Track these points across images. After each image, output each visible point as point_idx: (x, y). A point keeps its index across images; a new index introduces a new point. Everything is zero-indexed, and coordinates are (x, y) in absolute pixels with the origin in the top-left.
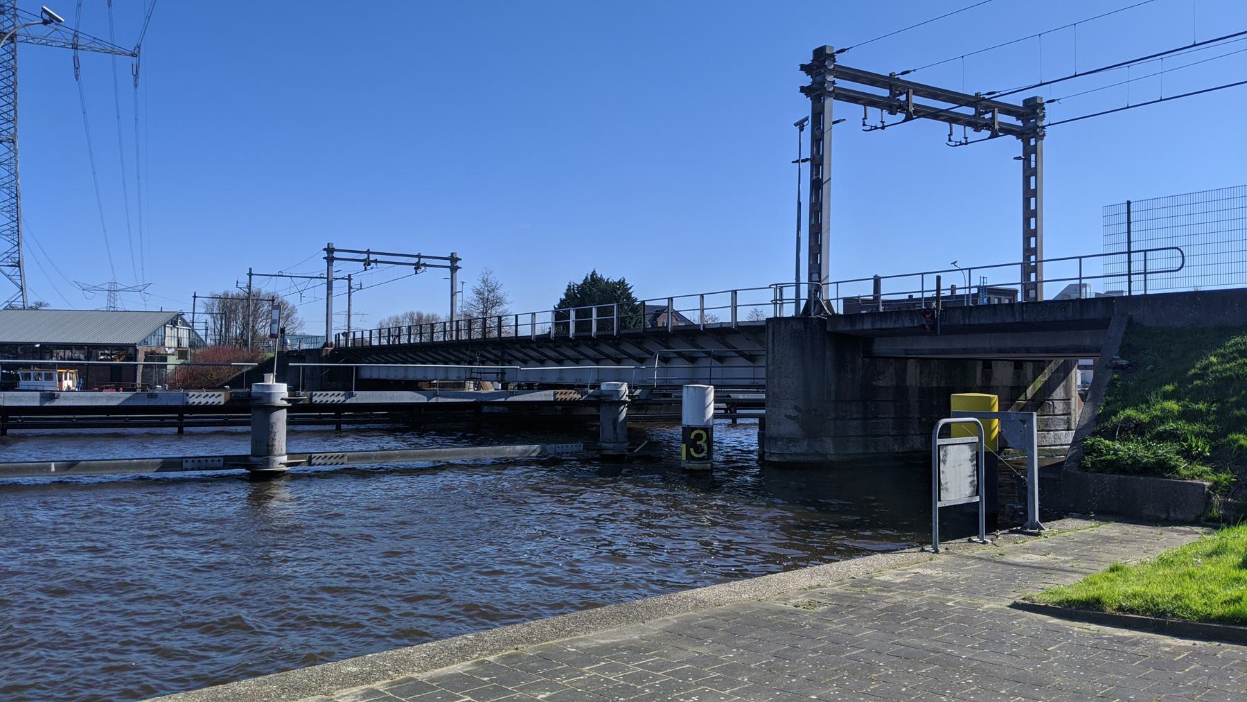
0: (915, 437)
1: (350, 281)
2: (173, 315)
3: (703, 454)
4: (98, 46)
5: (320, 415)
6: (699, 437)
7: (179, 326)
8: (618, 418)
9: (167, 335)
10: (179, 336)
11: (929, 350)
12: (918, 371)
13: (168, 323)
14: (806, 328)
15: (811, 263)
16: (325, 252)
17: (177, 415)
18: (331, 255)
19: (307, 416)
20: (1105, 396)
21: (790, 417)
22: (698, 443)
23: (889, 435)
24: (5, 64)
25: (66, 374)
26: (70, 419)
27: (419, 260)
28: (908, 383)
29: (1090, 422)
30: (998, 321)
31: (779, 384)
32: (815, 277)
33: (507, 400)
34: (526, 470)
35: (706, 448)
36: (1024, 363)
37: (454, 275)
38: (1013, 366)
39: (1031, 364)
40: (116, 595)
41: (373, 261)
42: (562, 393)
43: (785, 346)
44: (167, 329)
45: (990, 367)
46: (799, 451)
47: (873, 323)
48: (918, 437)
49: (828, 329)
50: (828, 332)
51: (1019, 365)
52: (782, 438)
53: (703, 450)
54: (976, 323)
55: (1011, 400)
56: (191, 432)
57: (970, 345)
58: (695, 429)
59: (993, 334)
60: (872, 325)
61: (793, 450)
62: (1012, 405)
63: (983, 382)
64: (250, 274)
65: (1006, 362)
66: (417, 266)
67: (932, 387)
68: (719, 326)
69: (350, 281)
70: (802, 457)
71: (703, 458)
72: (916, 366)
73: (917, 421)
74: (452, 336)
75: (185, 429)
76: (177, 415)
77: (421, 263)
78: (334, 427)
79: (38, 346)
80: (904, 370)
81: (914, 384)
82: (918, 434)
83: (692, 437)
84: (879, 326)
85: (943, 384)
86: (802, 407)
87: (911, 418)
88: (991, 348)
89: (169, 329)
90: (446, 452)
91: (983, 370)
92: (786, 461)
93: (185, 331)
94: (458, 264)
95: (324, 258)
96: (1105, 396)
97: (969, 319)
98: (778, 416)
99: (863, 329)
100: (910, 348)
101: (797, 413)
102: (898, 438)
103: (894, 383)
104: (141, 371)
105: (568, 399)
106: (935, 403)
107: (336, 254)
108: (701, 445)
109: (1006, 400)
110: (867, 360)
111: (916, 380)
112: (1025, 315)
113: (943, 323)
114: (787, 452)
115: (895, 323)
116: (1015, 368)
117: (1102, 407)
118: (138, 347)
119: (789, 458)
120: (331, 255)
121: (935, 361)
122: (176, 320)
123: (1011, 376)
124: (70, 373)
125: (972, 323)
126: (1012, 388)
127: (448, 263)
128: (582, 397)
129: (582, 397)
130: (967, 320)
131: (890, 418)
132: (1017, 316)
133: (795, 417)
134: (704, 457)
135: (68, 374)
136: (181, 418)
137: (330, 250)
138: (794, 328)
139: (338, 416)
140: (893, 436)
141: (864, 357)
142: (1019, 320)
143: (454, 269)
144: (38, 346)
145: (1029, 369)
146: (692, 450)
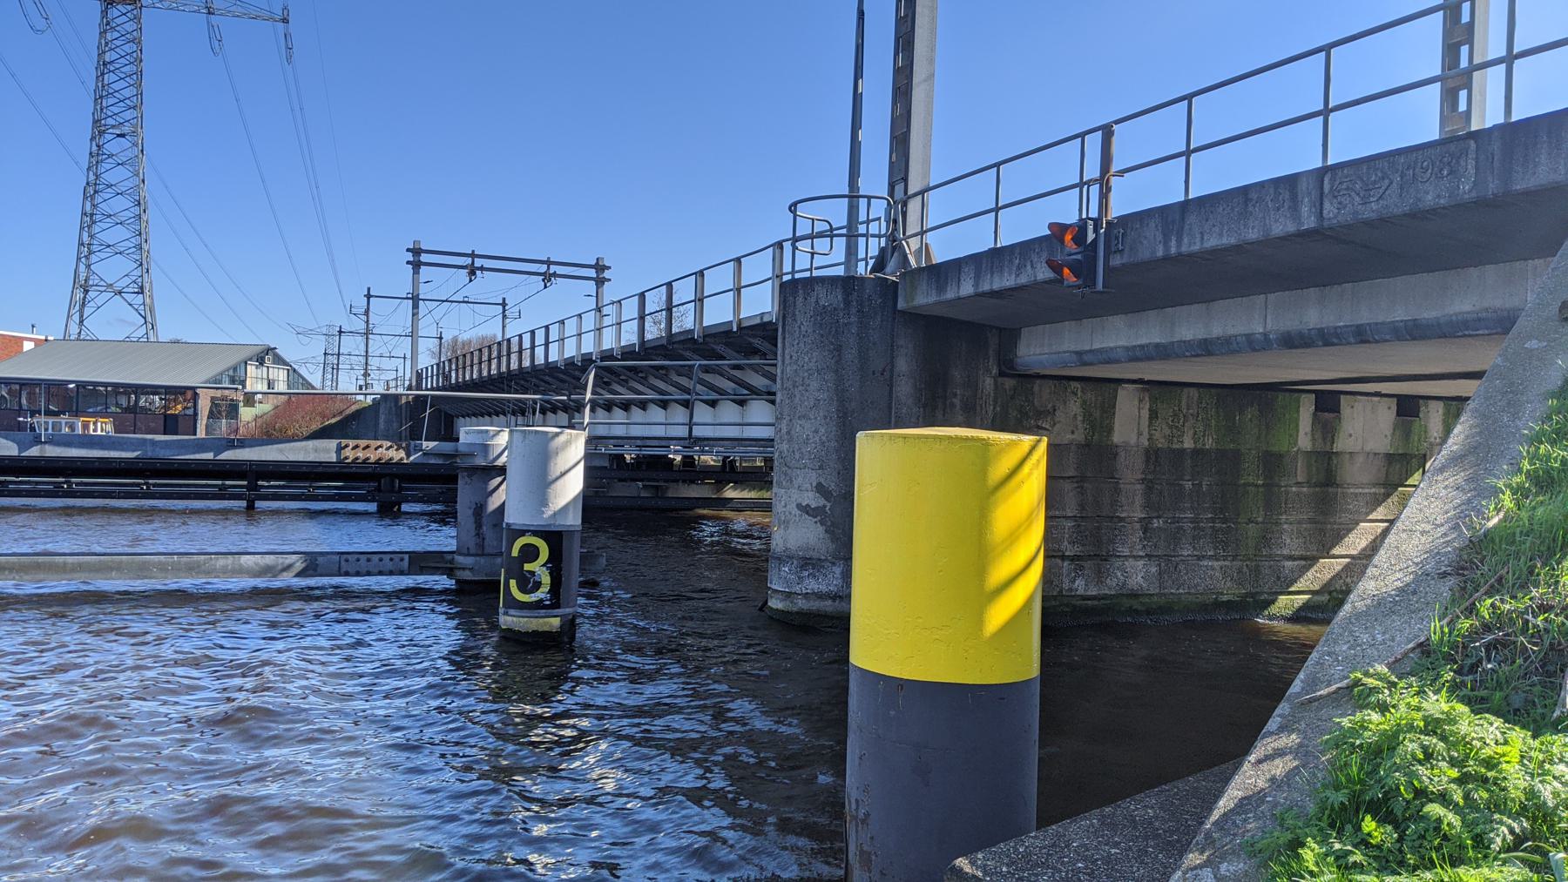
0: (1131, 562)
1: (504, 307)
2: (259, 349)
3: (542, 594)
4: (240, 9)
5: (223, 484)
6: (530, 553)
7: (268, 363)
8: (486, 502)
9: (248, 375)
10: (271, 377)
11: (1127, 348)
12: (1145, 413)
13: (251, 359)
14: (847, 303)
15: (894, 159)
16: (411, 254)
17: (246, 483)
18: (417, 259)
19: (180, 486)
20: (1536, 439)
21: (805, 509)
22: (527, 567)
23: (1063, 558)
24: (128, 36)
25: (95, 423)
26: (138, 485)
27: (549, 268)
28: (1117, 438)
29: (1423, 577)
30: (1253, 235)
31: (788, 433)
32: (899, 189)
33: (218, 458)
34: (94, 611)
35: (546, 579)
36: (1421, 401)
37: (600, 290)
38: (1394, 408)
39: (1440, 405)
40: (1067, 605)
41: (478, 269)
42: (356, 447)
43: (802, 345)
44: (248, 367)
45: (1336, 409)
46: (824, 588)
47: (977, 278)
48: (1140, 563)
49: (901, 305)
50: (903, 312)
51: (1408, 407)
52: (791, 557)
53: (538, 585)
54: (1196, 248)
55: (1384, 485)
56: (389, 511)
57: (1217, 331)
58: (522, 533)
59: (1272, 297)
60: (976, 285)
61: (812, 585)
62: (1388, 495)
63: (1314, 439)
64: (369, 296)
65: (1376, 399)
66: (548, 278)
67: (1183, 450)
68: (758, 321)
69: (504, 307)
70: (830, 602)
71: (538, 605)
72: (1141, 401)
73: (1138, 526)
74: (480, 371)
75: (258, 504)
76: (246, 483)
77: (551, 272)
78: (244, 504)
79: (72, 386)
80: (1109, 409)
81: (1133, 442)
82: (1141, 557)
83: (515, 553)
84: (986, 287)
85: (1209, 443)
86: (833, 486)
87: (1121, 519)
88: (1265, 335)
89: (254, 367)
90: (65, 564)
91: (1315, 414)
92: (795, 609)
93: (281, 371)
94: (607, 274)
95: (408, 263)
96: (1536, 439)
97: (1179, 242)
98: (785, 506)
99: (959, 298)
100: (1087, 348)
101: (822, 502)
102: (1088, 564)
103: (1079, 437)
104: (204, 422)
105: (372, 460)
106: (1188, 485)
107: (424, 258)
108: (533, 573)
109: (1375, 485)
110: (1009, 383)
111: (1140, 434)
112: (1327, 205)
113: (1116, 261)
114: (797, 589)
115: (1017, 276)
116: (1399, 414)
117: (1507, 501)
118: (198, 391)
119: (802, 604)
120: (417, 259)
121: (1194, 392)
122: (265, 355)
123: (1389, 433)
124: (102, 423)
125: (1184, 249)
126: (1390, 458)
127: (592, 273)
128: (408, 455)
129: (408, 455)
130: (1173, 243)
131: (1066, 517)
132: (1305, 210)
133: (817, 508)
134: (541, 601)
135: (99, 424)
136: (253, 487)
137: (416, 251)
138: (822, 303)
139: (253, 487)
140: (1073, 559)
141: (1002, 374)
142: (1309, 222)
143: (600, 282)
144: (72, 386)
145: (1434, 416)
146: (513, 583)
